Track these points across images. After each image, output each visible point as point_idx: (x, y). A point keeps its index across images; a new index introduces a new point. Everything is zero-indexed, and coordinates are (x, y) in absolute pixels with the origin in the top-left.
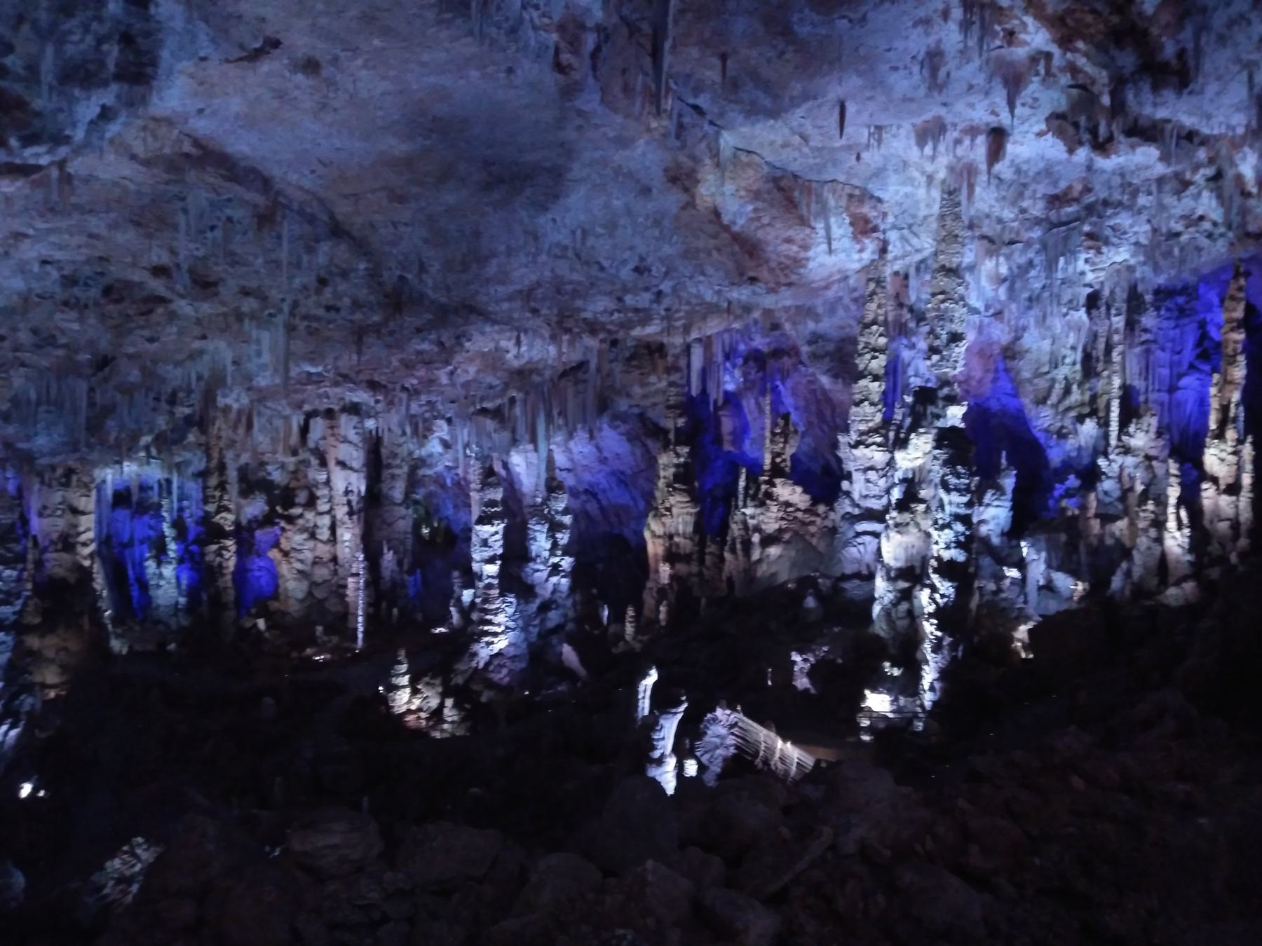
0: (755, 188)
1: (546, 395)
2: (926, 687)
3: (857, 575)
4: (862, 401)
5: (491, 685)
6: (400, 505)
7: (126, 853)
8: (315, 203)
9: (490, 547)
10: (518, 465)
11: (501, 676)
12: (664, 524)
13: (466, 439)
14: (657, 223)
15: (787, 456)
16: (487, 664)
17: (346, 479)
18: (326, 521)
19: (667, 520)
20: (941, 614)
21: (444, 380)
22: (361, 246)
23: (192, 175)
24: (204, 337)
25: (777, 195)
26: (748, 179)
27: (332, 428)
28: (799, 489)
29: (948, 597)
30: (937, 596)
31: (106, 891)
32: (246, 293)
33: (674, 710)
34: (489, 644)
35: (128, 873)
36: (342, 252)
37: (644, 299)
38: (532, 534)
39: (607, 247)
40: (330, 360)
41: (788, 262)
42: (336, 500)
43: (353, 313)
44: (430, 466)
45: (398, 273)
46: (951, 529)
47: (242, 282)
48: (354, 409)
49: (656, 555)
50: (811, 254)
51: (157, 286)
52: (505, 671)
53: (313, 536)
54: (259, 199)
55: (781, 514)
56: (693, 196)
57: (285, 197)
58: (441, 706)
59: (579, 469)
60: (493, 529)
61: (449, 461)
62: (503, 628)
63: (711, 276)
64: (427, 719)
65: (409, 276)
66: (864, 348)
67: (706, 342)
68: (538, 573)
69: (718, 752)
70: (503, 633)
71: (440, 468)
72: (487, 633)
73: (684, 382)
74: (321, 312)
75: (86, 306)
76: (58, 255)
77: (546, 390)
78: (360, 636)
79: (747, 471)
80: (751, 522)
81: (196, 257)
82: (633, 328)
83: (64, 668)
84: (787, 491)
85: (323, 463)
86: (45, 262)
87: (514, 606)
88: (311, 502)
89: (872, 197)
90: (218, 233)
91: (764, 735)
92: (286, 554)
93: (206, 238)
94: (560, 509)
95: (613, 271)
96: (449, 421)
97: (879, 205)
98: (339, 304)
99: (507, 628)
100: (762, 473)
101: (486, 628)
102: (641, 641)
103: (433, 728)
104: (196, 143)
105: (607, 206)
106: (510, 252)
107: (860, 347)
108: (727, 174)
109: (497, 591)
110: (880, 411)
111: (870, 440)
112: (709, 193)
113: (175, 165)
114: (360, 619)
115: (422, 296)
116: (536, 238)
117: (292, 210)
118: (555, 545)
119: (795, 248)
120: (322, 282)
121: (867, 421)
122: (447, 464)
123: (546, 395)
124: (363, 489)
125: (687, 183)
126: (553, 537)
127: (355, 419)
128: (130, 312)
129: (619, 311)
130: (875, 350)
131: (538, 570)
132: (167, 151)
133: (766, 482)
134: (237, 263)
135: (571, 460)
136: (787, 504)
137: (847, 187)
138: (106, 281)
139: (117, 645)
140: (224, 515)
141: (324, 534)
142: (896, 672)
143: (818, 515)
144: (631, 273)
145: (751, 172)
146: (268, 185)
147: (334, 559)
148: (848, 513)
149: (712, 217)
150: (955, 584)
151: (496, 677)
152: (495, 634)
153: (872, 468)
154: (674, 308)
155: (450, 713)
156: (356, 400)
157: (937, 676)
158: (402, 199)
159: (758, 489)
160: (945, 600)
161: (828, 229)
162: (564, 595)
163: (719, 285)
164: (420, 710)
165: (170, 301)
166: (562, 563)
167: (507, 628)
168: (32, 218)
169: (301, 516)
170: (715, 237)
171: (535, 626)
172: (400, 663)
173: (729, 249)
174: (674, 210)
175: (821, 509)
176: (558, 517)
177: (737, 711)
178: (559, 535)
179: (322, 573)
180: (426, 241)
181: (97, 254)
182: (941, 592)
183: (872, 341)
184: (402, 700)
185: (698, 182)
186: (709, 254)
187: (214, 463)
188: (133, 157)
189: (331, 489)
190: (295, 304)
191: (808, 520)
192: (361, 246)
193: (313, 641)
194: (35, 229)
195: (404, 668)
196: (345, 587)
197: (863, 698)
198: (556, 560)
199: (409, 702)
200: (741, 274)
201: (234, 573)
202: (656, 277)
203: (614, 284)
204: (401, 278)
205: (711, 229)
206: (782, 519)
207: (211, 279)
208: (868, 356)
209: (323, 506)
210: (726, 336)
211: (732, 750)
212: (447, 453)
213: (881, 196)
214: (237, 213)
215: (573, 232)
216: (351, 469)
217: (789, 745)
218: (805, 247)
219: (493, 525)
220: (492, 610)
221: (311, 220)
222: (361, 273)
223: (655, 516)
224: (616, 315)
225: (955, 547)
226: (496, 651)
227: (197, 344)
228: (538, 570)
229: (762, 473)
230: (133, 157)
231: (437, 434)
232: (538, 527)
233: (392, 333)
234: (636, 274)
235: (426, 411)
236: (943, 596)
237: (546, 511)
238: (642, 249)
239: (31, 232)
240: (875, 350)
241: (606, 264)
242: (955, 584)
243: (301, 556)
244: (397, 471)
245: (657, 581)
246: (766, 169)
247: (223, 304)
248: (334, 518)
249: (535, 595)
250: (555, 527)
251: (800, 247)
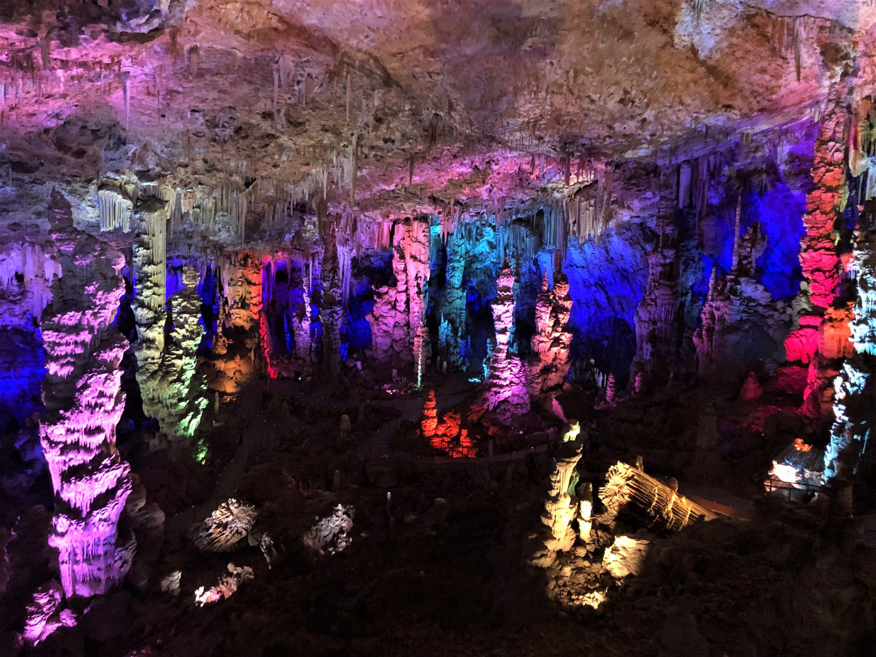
0: (730, 25)
1: (565, 207)
2: (827, 463)
3: (799, 363)
4: (815, 210)
5: (495, 423)
6: (457, 289)
7: (224, 507)
8: (372, 61)
11: (505, 418)
12: (649, 312)
14: (638, 61)
15: (753, 259)
16: (495, 408)
17: (416, 268)
18: (403, 297)
19: (652, 309)
20: (849, 401)
21: (485, 196)
22: (406, 92)
23: (279, 44)
24: (308, 164)
25: (752, 31)
26: (724, 18)
27: (409, 231)
28: (761, 288)
29: (859, 386)
30: (848, 385)
31: (211, 531)
32: (325, 130)
33: (568, 460)
34: (497, 393)
35: (224, 521)
36: (393, 96)
37: (631, 126)
38: (538, 314)
39: (595, 84)
40: (397, 181)
41: (761, 90)
42: (410, 284)
43: (402, 144)
44: (482, 261)
45: (434, 112)
46: (867, 324)
47: (323, 122)
48: (424, 218)
49: (642, 336)
50: (782, 82)
51: (266, 126)
52: (508, 414)
53: (394, 307)
54: (330, 60)
55: (742, 308)
56: (672, 37)
57: (349, 58)
58: (460, 434)
59: (591, 266)
60: (504, 309)
62: (508, 382)
63: (688, 105)
64: (449, 443)
65: (442, 114)
66: (820, 162)
67: (694, 164)
68: (542, 343)
69: (616, 498)
70: (507, 385)
71: (488, 263)
72: (495, 385)
73: (673, 197)
74: (381, 143)
75: (225, 142)
76: (201, 106)
77: (564, 203)
78: (419, 379)
79: (716, 270)
80: (717, 314)
81: (290, 104)
82: (625, 151)
83: (238, 384)
84: (750, 289)
85: (402, 257)
86: (193, 111)
87: (519, 367)
88: (394, 283)
89: (843, 28)
90: (302, 86)
91: (656, 487)
92: (376, 319)
93: (294, 90)
95: (602, 103)
96: (494, 228)
97: (850, 35)
98: (393, 137)
99: (511, 382)
100: (730, 272)
101: (495, 381)
102: (618, 403)
103: (452, 449)
104: (281, 19)
105: (595, 49)
106: (517, 91)
107: (816, 161)
108: (702, 15)
109: (505, 355)
110: (832, 219)
111: (820, 245)
112: (686, 33)
113: (266, 35)
114: (420, 367)
115: (451, 129)
116: (537, 79)
117: (354, 67)
118: (557, 323)
119: (767, 77)
120: (379, 120)
121: (818, 228)
123: (565, 207)
124: (428, 276)
125: (665, 26)
127: (424, 226)
128: (256, 146)
129: (610, 137)
130: (830, 164)
131: (542, 342)
132: (259, 26)
133: (731, 280)
134: (317, 108)
135: (585, 259)
136: (750, 299)
137: (817, 20)
138: (236, 124)
139: (272, 372)
140: (334, 289)
141: (402, 306)
142: (806, 448)
143: (776, 310)
144: (617, 105)
145: (725, 12)
146: (335, 47)
147: (408, 324)
148: (804, 309)
149: (690, 54)
150: (866, 375)
151: (501, 418)
152: (502, 386)
153: (818, 270)
154: (658, 133)
155: (465, 441)
156: (424, 211)
157: (836, 455)
158: (433, 54)
159: (725, 286)
160: (855, 388)
161: (798, 58)
162: (563, 362)
163: (696, 113)
164: (444, 435)
165: (279, 137)
166: (563, 337)
167: (511, 382)
168: (180, 80)
169: (387, 293)
170: (692, 71)
171: (538, 383)
172: (430, 400)
173: (705, 81)
174: (654, 51)
175: (780, 305)
176: (561, 302)
177: (635, 466)
178: (561, 316)
179: (399, 333)
180: (453, 85)
181: (227, 105)
182: (853, 381)
183: (829, 156)
184: (431, 426)
185: (675, 24)
186: (687, 86)
187: (330, 254)
188: (238, 32)
189: (407, 275)
190: (360, 138)
191: (766, 314)
192: (406, 92)
193: (389, 380)
194: (183, 88)
195: (433, 404)
196: (413, 344)
197: (771, 467)
198: (557, 335)
199: (436, 428)
200: (717, 103)
201: (341, 329)
202: (639, 107)
203: (603, 114)
204: (437, 115)
205: (688, 65)
206: (744, 311)
207: (300, 120)
208: (823, 170)
209: (401, 287)
210: (712, 158)
211: (627, 498)
213: (852, 27)
214: (315, 71)
215: (567, 72)
216: (420, 261)
217: (684, 499)
218: (777, 76)
219: (505, 305)
220: (499, 368)
221: (370, 74)
222: (406, 113)
223: (642, 305)
224: (608, 140)
225: (869, 341)
226: (502, 399)
227: (304, 169)
229: (730, 272)
230: (238, 32)
231: (485, 238)
232: (543, 309)
233: (435, 159)
234: (621, 105)
235: (477, 221)
236: (853, 385)
237: (551, 297)
238: (626, 84)
239: (180, 89)
240: (830, 164)
241: (595, 97)
242: (866, 375)
243: (386, 321)
244: (456, 265)
245: (641, 357)
246: (741, 8)
247: (311, 138)
248: (408, 295)
249: (540, 360)
250: (557, 310)
251: (772, 76)
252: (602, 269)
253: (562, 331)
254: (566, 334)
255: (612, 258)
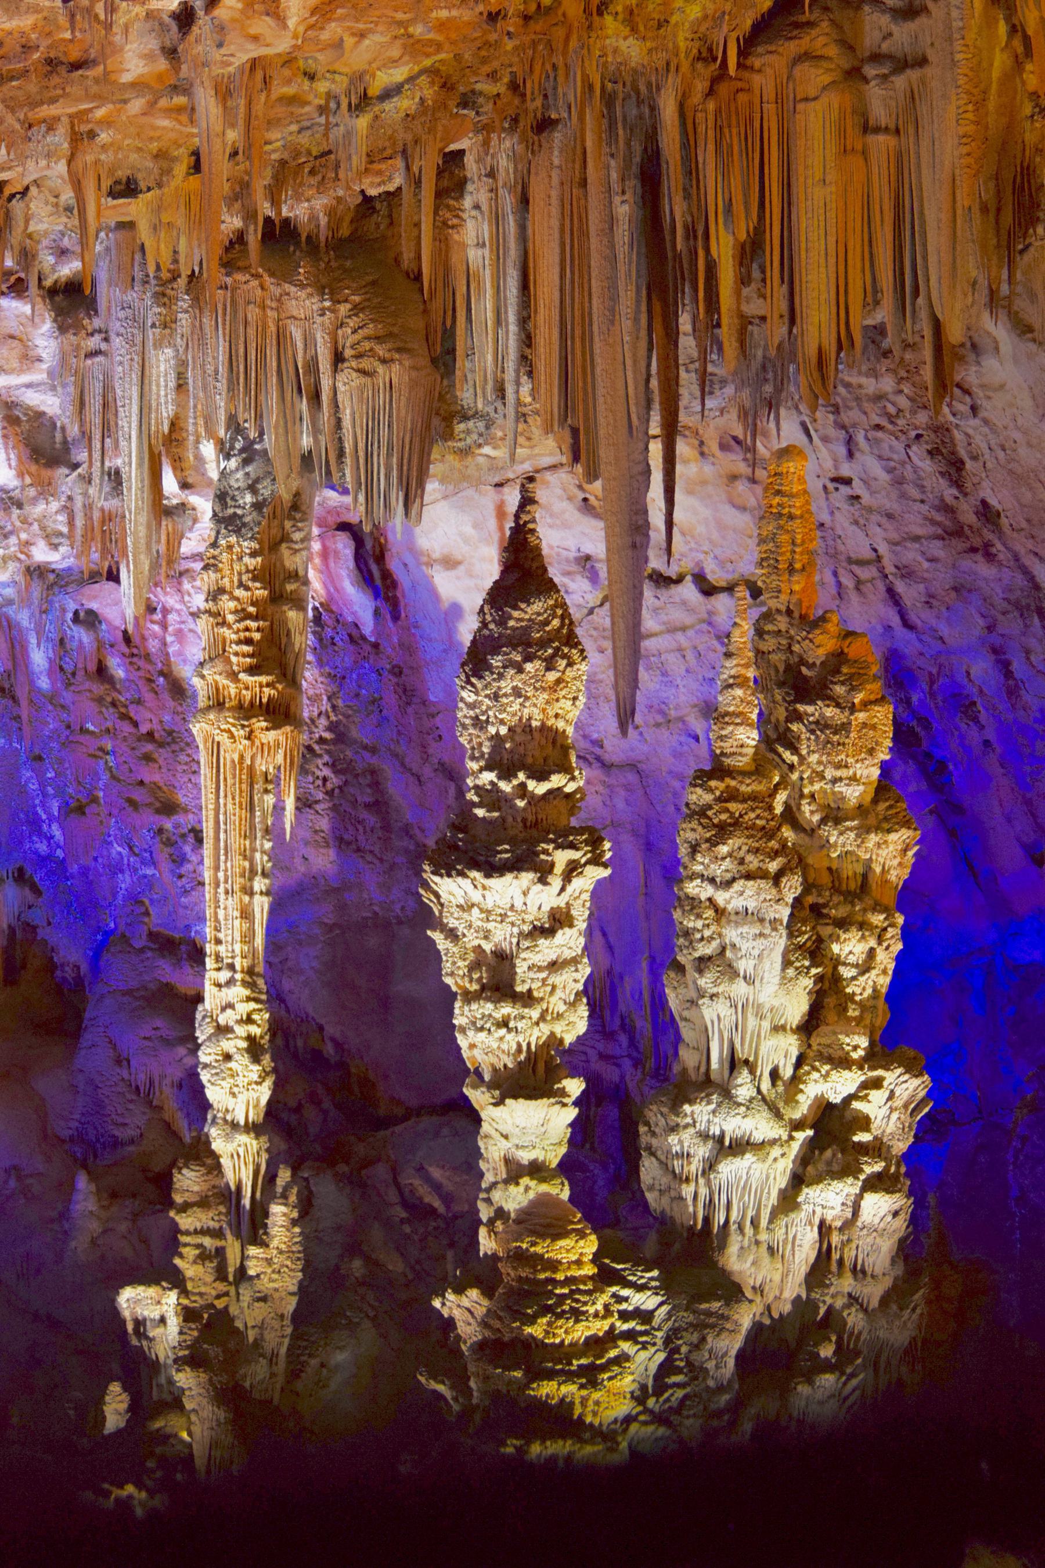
9: (528, 999)
10: (450, 563)
13: (166, 410)
61: (53, 540)
94: (853, 794)
122: (42, 554)
126: (816, 952)
131: (739, 1147)
162: (873, 1292)
166: (874, 1106)
212: (46, 489)
220: (563, 1353)
228: (739, 1147)
252: (910, 593)
253: (874, 1058)
254: (891, 1077)
255: (987, 513)
